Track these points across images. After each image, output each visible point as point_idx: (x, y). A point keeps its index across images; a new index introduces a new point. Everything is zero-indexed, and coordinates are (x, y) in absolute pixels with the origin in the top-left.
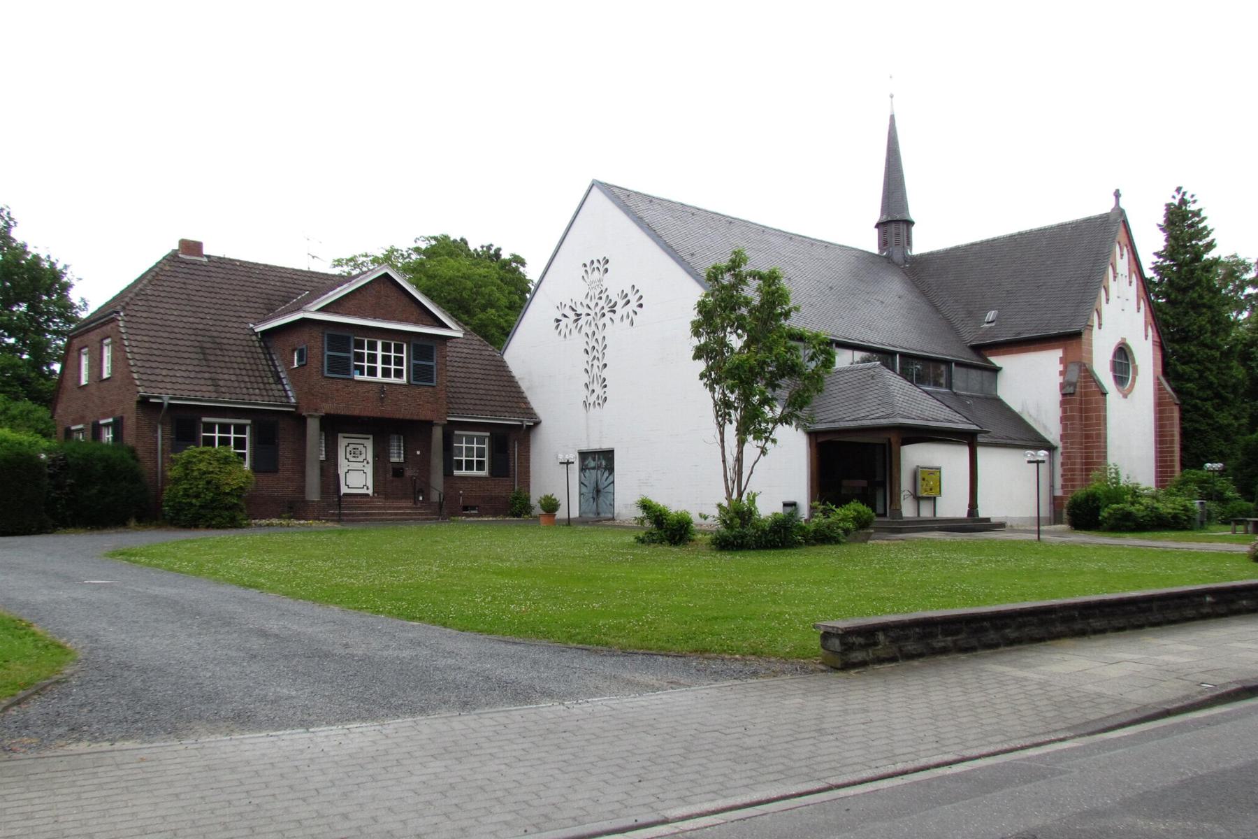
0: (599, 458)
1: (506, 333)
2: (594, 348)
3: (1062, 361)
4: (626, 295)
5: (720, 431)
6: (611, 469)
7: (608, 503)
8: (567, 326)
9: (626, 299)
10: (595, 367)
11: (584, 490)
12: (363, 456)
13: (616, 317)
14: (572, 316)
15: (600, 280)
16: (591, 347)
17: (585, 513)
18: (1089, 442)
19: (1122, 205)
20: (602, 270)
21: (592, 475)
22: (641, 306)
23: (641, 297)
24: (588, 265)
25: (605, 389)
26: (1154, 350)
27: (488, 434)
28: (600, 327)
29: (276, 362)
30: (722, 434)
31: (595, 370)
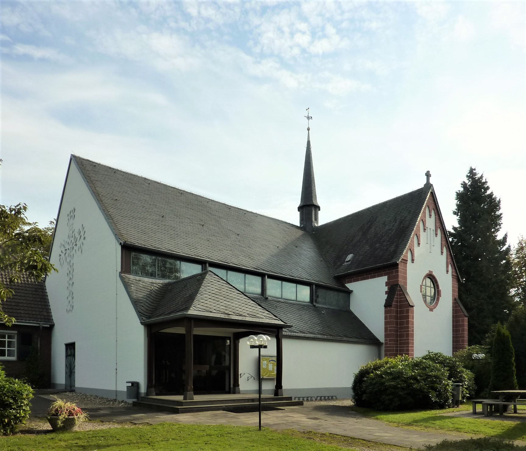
18: (403, 340)
19: (431, 182)
26: (453, 281)
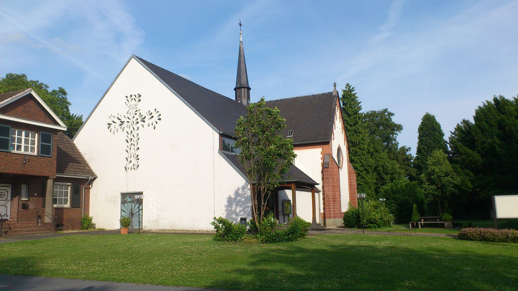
2: (131, 139)
3: (322, 153)
4: (151, 113)
13: (145, 124)
14: (119, 122)
15: (136, 105)
16: (129, 138)
21: (129, 206)
22: (160, 119)
24: (129, 96)
25: (138, 161)
27: (70, 184)
28: (136, 129)
31: (132, 150)
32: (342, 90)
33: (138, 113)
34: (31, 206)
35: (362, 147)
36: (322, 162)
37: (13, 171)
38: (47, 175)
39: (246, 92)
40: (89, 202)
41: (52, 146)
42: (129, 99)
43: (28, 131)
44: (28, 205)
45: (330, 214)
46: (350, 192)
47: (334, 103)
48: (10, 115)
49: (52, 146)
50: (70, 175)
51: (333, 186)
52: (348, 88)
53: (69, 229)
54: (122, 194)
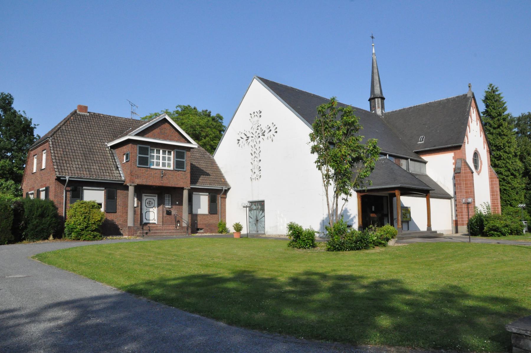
0: (257, 205)
1: (213, 149)
3: (454, 158)
4: (270, 127)
5: (326, 189)
6: (263, 210)
7: (262, 226)
8: (242, 142)
9: (270, 129)
10: (255, 161)
11: (251, 220)
12: (153, 205)
14: (245, 138)
15: (258, 121)
17: (251, 231)
20: (258, 116)
21: (254, 213)
22: (276, 132)
23: (276, 128)
27: (208, 194)
28: (258, 142)
29: (116, 160)
30: (327, 191)
32: (485, 91)
33: (259, 128)
34: (173, 212)
35: (507, 150)
36: (454, 167)
37: (152, 183)
38: (182, 186)
39: (380, 102)
40: (225, 209)
41: (185, 161)
42: (253, 116)
43: (170, 150)
44: (171, 212)
45: (462, 221)
46: (492, 197)
47: (469, 105)
48: (180, 140)
49: (185, 161)
50: (206, 186)
51: (466, 192)
52: (491, 88)
53: (208, 232)
54: (263, 201)
